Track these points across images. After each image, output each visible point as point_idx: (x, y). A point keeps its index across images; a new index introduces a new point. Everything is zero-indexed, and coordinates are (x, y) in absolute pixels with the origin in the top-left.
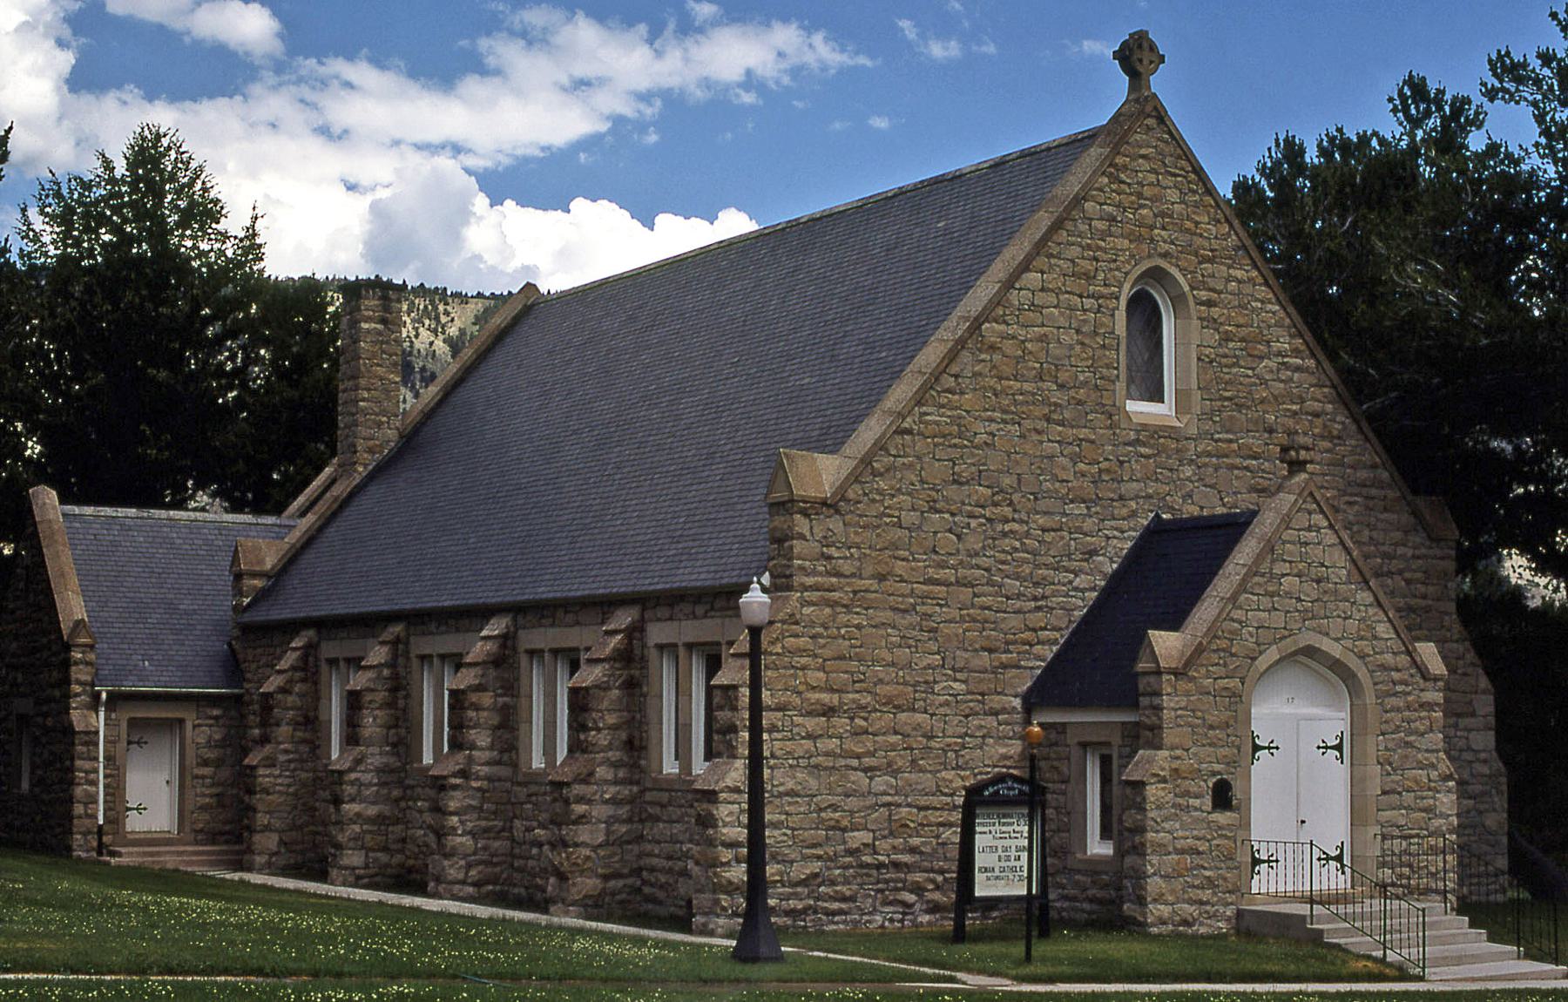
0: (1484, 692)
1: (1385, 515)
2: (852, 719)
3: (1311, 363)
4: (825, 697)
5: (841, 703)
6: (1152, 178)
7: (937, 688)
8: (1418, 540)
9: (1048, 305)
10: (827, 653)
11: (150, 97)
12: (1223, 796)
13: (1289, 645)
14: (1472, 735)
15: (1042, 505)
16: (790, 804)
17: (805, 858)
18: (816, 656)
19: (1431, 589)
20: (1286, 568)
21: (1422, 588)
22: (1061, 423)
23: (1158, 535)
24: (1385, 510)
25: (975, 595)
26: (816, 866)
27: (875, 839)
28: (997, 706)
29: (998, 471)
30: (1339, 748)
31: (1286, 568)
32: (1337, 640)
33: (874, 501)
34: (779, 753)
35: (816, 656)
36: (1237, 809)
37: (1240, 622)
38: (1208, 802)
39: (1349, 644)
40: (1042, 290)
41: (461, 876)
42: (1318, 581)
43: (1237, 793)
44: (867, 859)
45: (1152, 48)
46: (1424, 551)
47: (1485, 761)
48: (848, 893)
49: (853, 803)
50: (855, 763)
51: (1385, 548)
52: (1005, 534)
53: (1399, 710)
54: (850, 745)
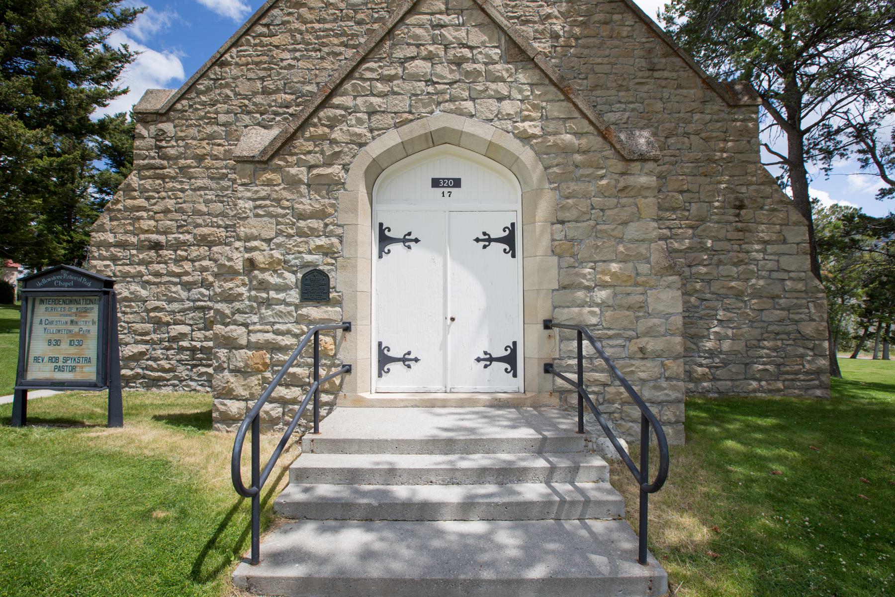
0: (796, 224)
1: (678, 92)
2: (175, 251)
4: (154, 237)
5: (168, 241)
8: (716, 108)
10: (156, 208)
12: (316, 287)
14: (782, 259)
16: (126, 307)
17: (137, 342)
18: (149, 210)
24: (680, 87)
26: (142, 348)
27: (193, 331)
29: (299, 82)
30: (509, 240)
31: (411, 51)
33: (197, 109)
34: (118, 274)
35: (149, 210)
36: (338, 303)
37: (346, 109)
43: (337, 280)
44: (185, 344)
46: (723, 115)
47: (800, 279)
48: (167, 366)
49: (176, 306)
53: (586, 196)
54: (174, 268)
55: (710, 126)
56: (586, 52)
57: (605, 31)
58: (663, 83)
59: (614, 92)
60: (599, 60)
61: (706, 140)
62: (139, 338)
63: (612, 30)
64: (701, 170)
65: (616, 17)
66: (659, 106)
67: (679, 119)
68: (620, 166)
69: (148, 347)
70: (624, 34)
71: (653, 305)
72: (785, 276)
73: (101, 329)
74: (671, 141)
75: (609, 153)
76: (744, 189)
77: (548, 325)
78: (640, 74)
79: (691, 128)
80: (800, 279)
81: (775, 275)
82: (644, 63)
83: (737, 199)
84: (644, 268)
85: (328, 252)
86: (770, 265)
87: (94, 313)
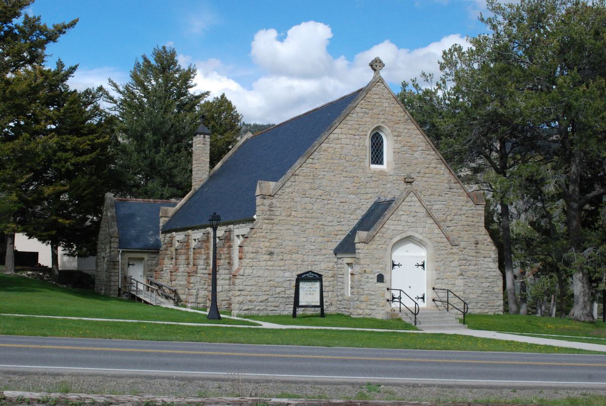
1: (459, 197)
3: (434, 152)
6: (379, 100)
7: (306, 247)
9: (346, 139)
11: (462, 37)
13: (404, 235)
15: (341, 195)
19: (475, 219)
20: (403, 213)
21: (472, 219)
22: (346, 172)
23: (377, 204)
24: (459, 196)
25: (318, 221)
28: (325, 253)
30: (423, 265)
31: (403, 213)
32: (421, 234)
38: (376, 280)
39: (425, 235)
40: (341, 134)
41: (194, 301)
42: (414, 217)
45: (380, 62)
46: (473, 208)
47: (495, 271)
50: (279, 268)
51: (459, 207)
52: (328, 204)
55: (469, 212)
56: (428, 179)
57: (435, 171)
58: (454, 194)
59: (437, 197)
60: (433, 184)
61: (467, 217)
62: (264, 293)
63: (437, 171)
64: (465, 229)
65: (439, 166)
66: (452, 203)
67: (458, 209)
68: (451, 247)
69: (268, 296)
70: (442, 173)
71: (457, 283)
72: (490, 270)
73: (75, 293)
74: (455, 217)
75: (448, 243)
76: (478, 237)
77: (434, 289)
78: (446, 190)
79: (462, 212)
80: (495, 271)
81: (487, 270)
82: (447, 185)
83: (476, 241)
84: (455, 274)
85: (382, 269)
86: (486, 266)
87: (318, 284)
